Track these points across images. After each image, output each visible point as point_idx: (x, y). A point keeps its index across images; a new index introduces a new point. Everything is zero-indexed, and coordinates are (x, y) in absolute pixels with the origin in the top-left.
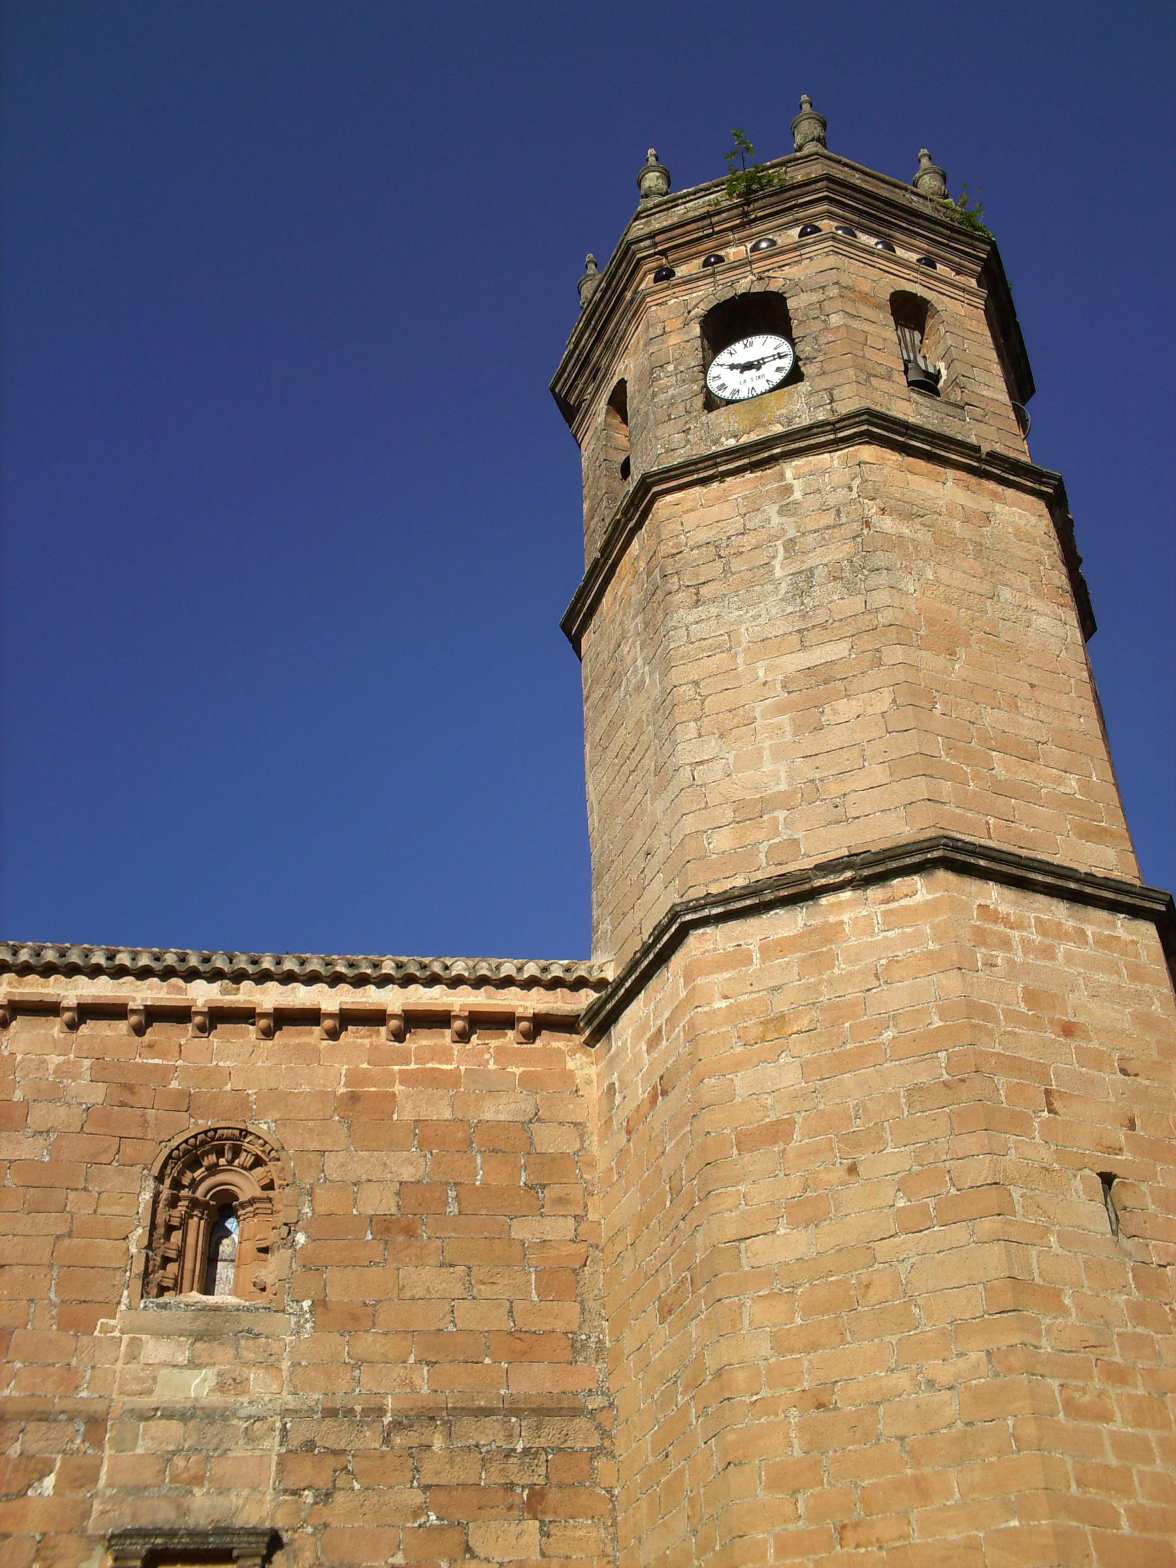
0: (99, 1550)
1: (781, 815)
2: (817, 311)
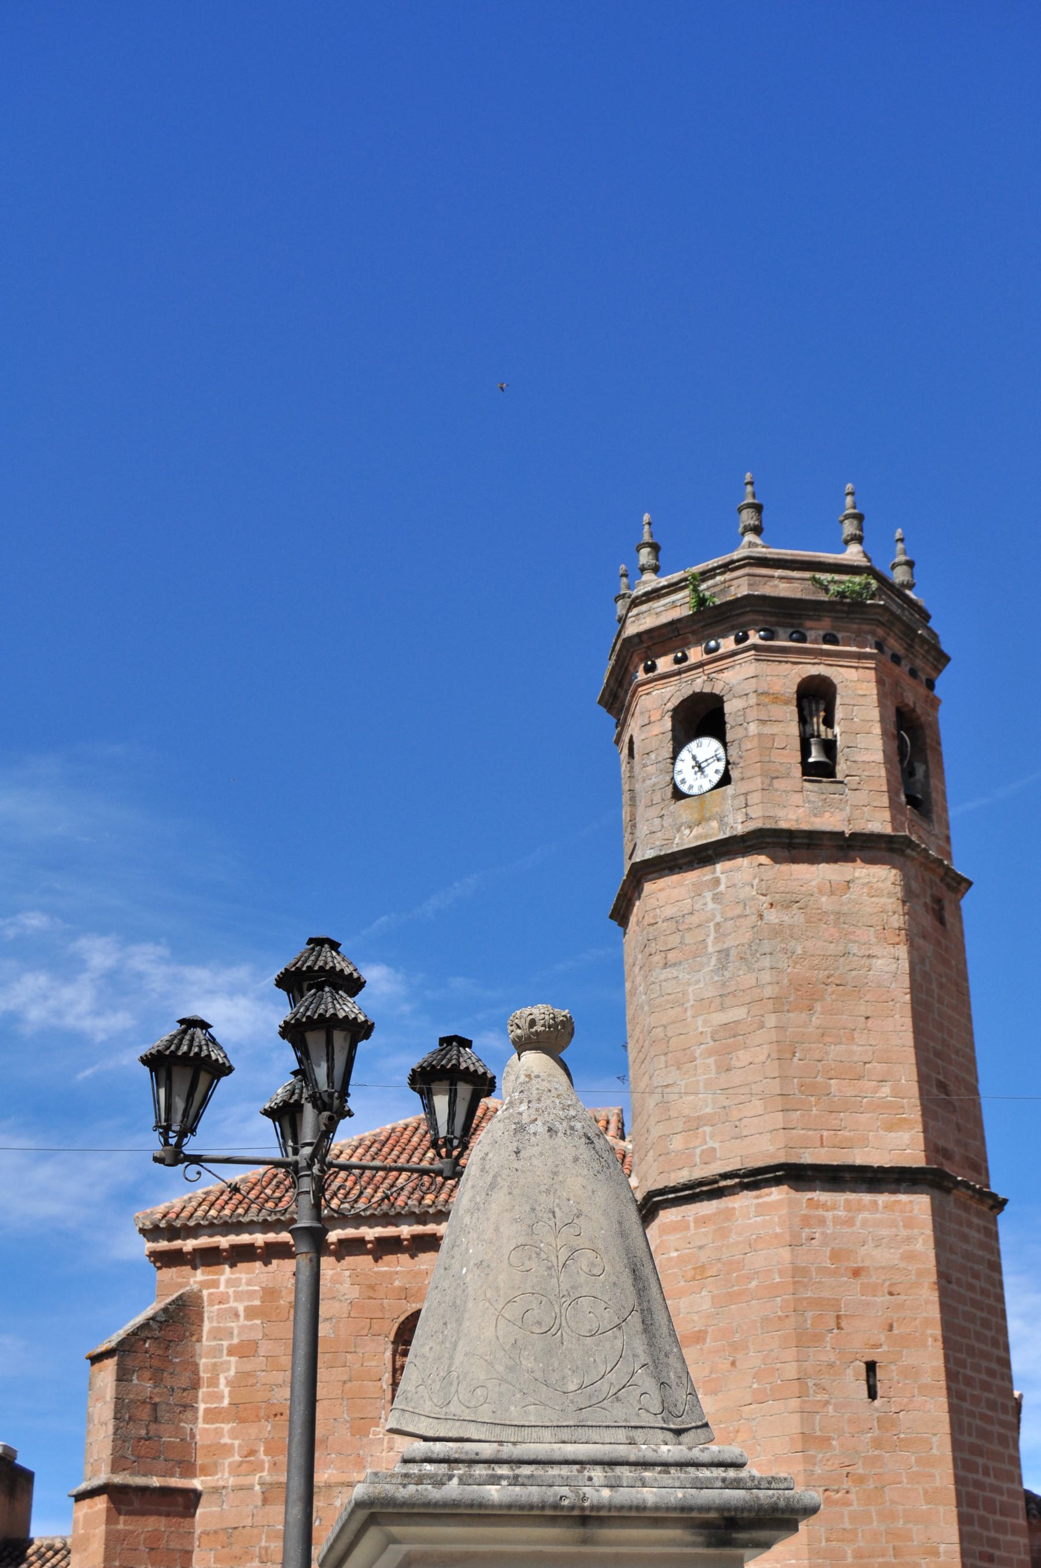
1: (708, 1129)
2: (742, 718)
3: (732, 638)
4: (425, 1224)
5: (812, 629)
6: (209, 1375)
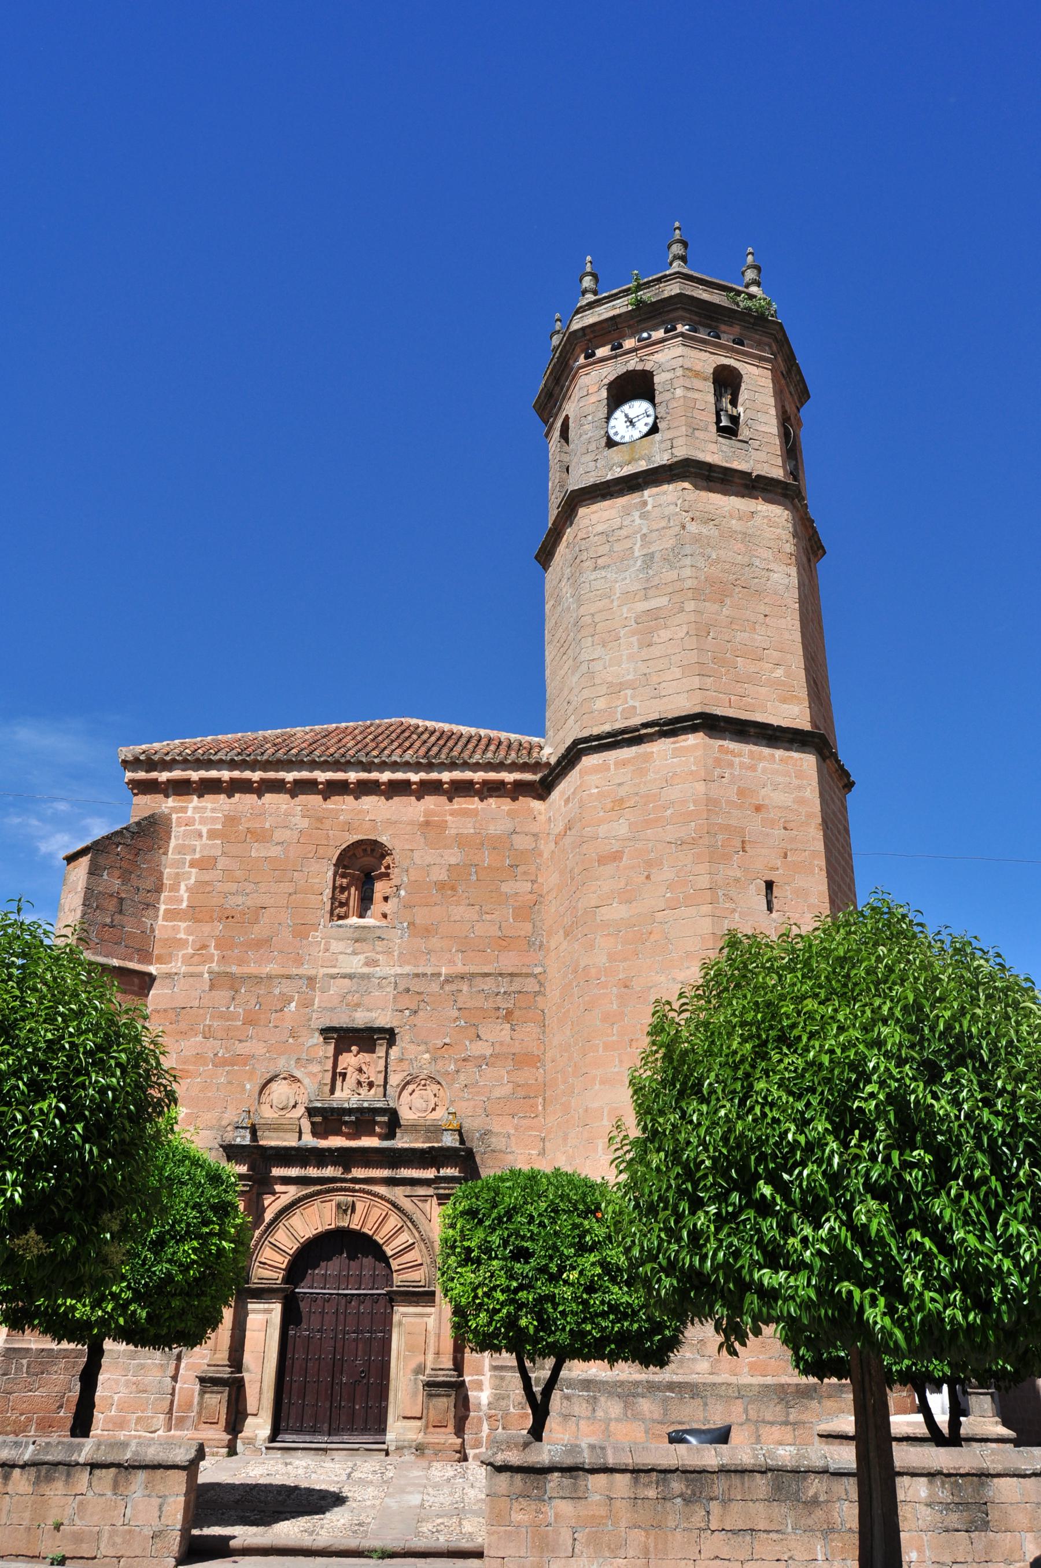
0: (317, 1034)
1: (629, 692)
3: (662, 331)
4: (370, 772)
5: (724, 332)
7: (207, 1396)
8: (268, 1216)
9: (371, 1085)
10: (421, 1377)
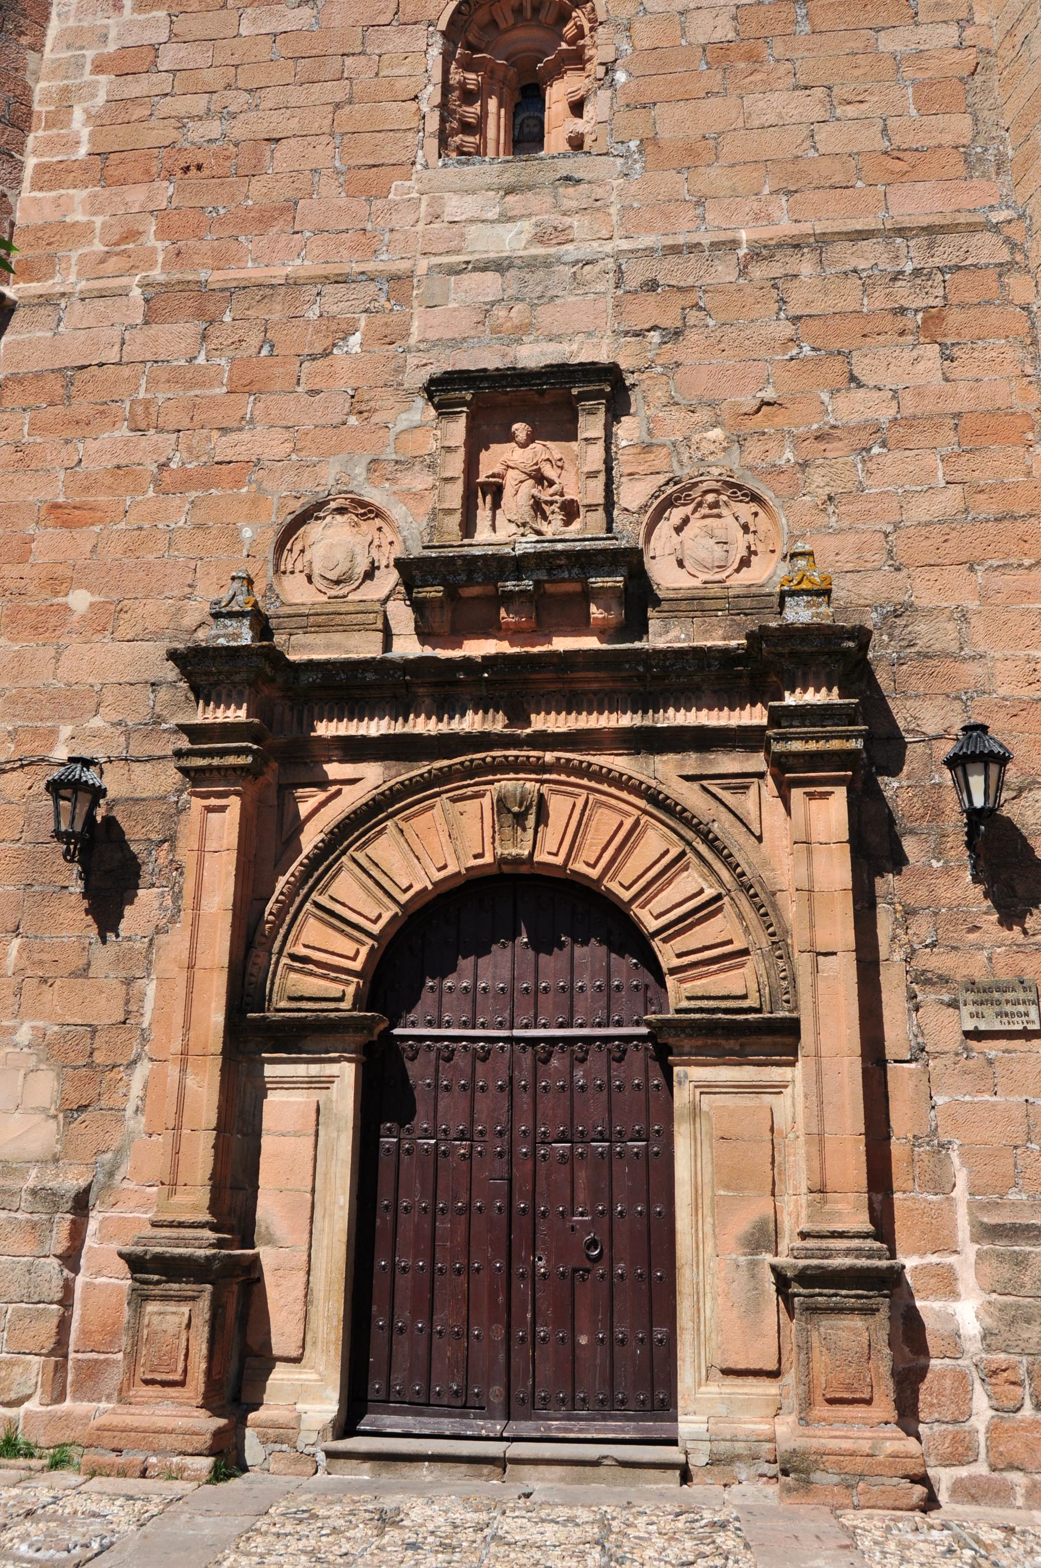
0: (420, 402)
6: (53, 108)
7: (151, 1307)
8: (310, 839)
9: (570, 511)
10: (769, 1258)
